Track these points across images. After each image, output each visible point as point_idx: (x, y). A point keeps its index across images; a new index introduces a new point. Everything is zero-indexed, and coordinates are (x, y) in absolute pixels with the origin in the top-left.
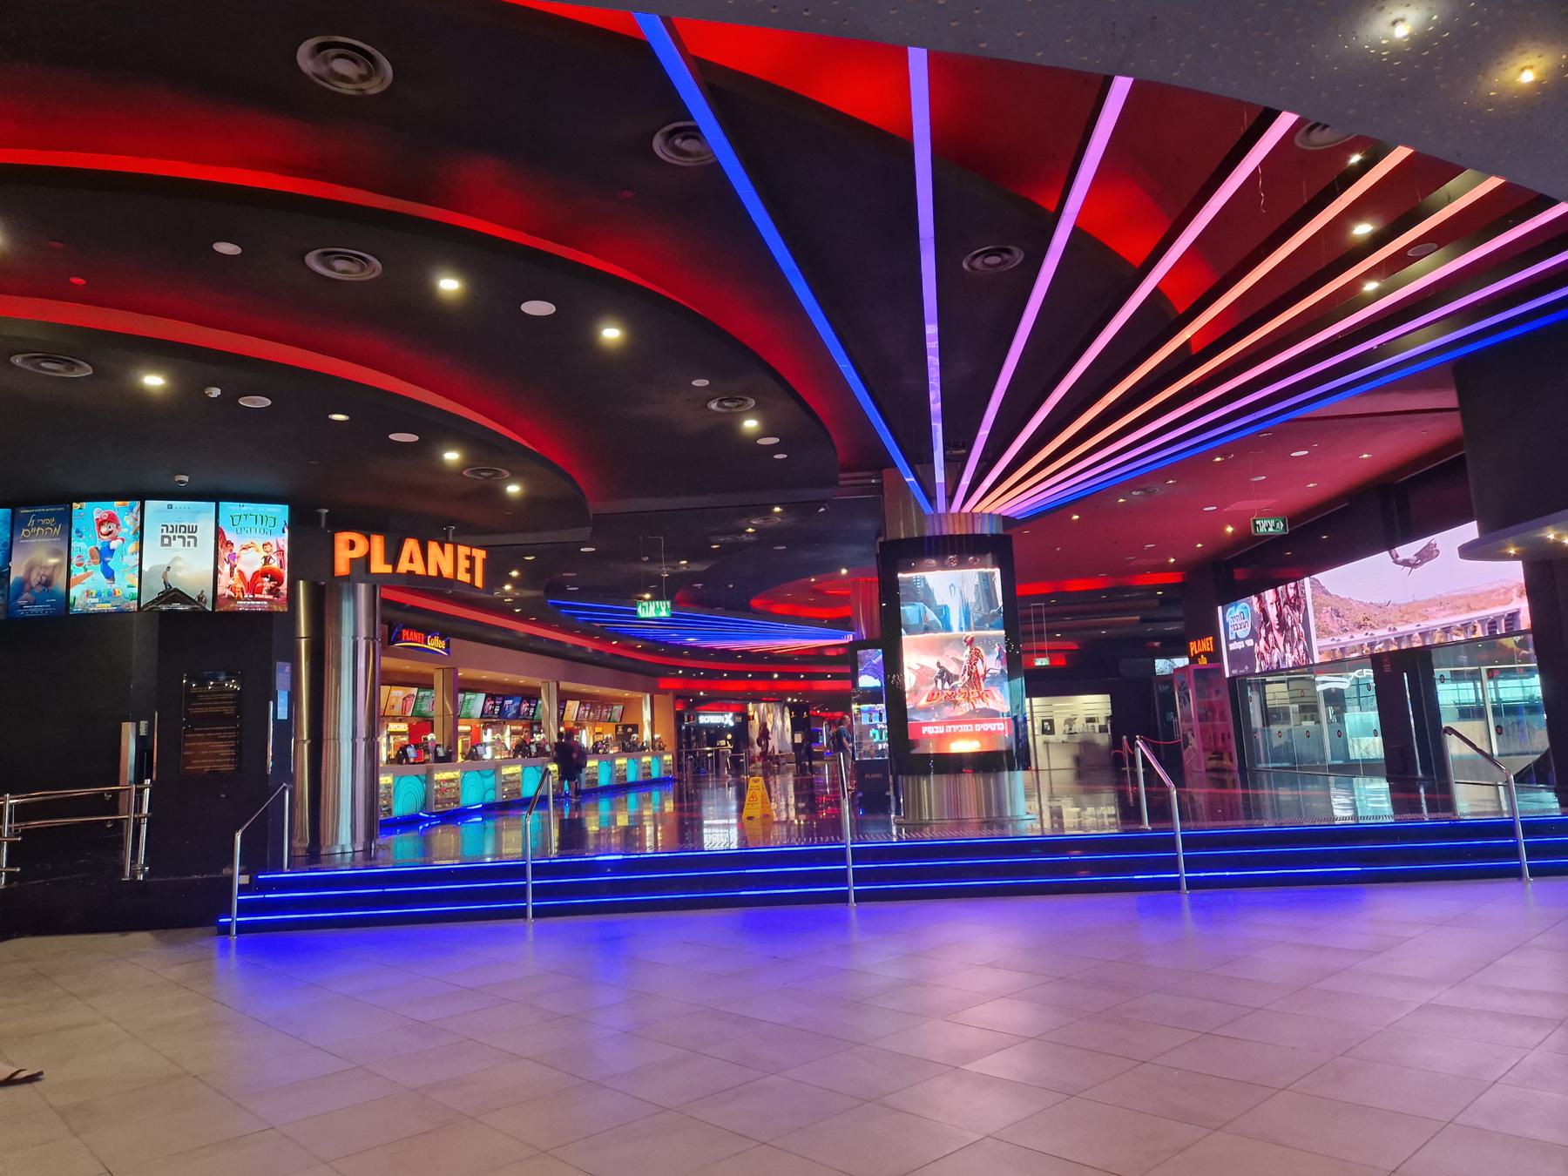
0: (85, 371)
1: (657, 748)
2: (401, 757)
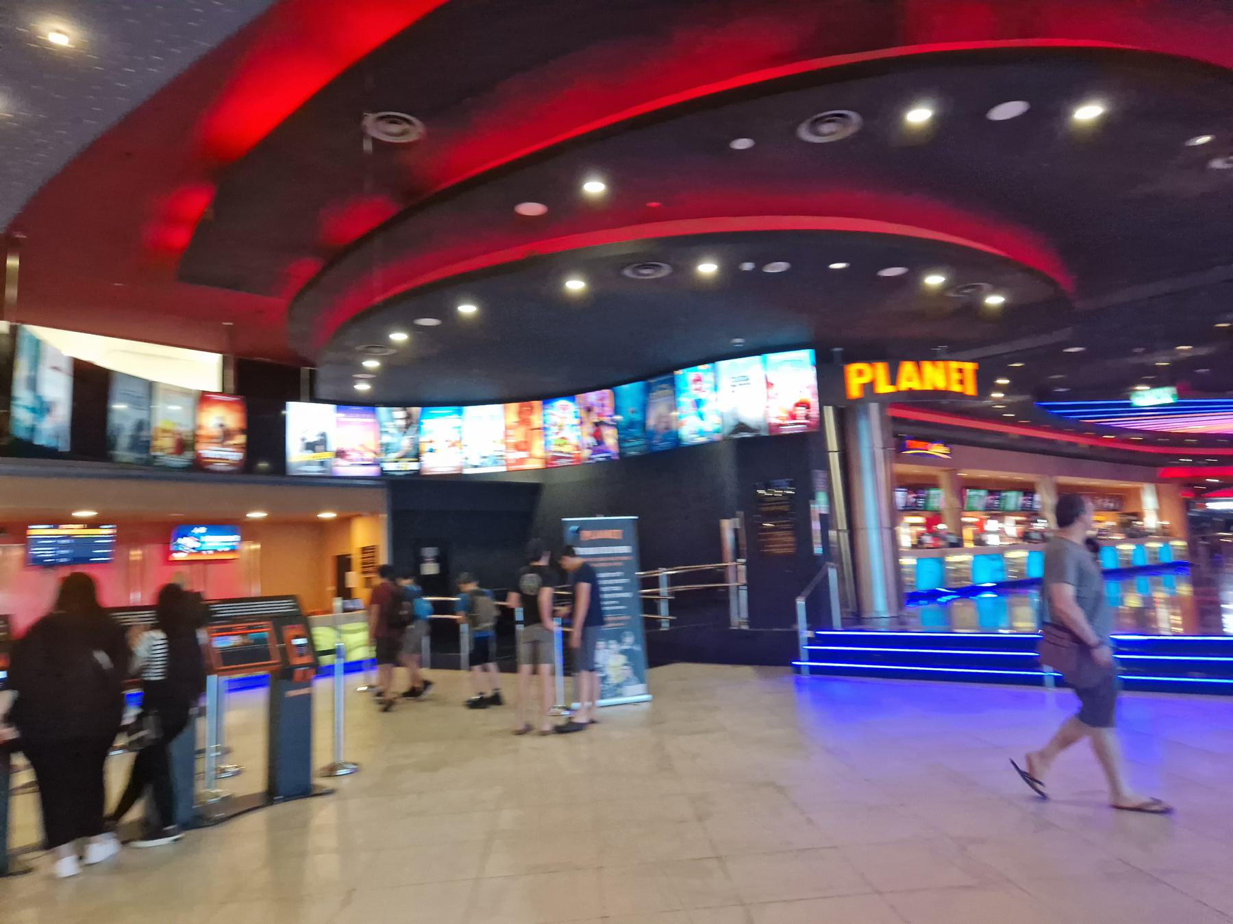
0: (665, 271)
1: (1164, 534)
2: (918, 545)
